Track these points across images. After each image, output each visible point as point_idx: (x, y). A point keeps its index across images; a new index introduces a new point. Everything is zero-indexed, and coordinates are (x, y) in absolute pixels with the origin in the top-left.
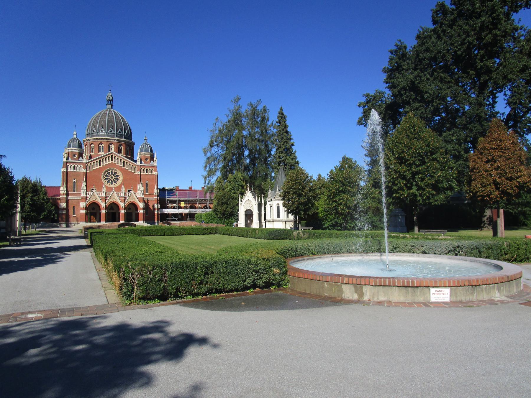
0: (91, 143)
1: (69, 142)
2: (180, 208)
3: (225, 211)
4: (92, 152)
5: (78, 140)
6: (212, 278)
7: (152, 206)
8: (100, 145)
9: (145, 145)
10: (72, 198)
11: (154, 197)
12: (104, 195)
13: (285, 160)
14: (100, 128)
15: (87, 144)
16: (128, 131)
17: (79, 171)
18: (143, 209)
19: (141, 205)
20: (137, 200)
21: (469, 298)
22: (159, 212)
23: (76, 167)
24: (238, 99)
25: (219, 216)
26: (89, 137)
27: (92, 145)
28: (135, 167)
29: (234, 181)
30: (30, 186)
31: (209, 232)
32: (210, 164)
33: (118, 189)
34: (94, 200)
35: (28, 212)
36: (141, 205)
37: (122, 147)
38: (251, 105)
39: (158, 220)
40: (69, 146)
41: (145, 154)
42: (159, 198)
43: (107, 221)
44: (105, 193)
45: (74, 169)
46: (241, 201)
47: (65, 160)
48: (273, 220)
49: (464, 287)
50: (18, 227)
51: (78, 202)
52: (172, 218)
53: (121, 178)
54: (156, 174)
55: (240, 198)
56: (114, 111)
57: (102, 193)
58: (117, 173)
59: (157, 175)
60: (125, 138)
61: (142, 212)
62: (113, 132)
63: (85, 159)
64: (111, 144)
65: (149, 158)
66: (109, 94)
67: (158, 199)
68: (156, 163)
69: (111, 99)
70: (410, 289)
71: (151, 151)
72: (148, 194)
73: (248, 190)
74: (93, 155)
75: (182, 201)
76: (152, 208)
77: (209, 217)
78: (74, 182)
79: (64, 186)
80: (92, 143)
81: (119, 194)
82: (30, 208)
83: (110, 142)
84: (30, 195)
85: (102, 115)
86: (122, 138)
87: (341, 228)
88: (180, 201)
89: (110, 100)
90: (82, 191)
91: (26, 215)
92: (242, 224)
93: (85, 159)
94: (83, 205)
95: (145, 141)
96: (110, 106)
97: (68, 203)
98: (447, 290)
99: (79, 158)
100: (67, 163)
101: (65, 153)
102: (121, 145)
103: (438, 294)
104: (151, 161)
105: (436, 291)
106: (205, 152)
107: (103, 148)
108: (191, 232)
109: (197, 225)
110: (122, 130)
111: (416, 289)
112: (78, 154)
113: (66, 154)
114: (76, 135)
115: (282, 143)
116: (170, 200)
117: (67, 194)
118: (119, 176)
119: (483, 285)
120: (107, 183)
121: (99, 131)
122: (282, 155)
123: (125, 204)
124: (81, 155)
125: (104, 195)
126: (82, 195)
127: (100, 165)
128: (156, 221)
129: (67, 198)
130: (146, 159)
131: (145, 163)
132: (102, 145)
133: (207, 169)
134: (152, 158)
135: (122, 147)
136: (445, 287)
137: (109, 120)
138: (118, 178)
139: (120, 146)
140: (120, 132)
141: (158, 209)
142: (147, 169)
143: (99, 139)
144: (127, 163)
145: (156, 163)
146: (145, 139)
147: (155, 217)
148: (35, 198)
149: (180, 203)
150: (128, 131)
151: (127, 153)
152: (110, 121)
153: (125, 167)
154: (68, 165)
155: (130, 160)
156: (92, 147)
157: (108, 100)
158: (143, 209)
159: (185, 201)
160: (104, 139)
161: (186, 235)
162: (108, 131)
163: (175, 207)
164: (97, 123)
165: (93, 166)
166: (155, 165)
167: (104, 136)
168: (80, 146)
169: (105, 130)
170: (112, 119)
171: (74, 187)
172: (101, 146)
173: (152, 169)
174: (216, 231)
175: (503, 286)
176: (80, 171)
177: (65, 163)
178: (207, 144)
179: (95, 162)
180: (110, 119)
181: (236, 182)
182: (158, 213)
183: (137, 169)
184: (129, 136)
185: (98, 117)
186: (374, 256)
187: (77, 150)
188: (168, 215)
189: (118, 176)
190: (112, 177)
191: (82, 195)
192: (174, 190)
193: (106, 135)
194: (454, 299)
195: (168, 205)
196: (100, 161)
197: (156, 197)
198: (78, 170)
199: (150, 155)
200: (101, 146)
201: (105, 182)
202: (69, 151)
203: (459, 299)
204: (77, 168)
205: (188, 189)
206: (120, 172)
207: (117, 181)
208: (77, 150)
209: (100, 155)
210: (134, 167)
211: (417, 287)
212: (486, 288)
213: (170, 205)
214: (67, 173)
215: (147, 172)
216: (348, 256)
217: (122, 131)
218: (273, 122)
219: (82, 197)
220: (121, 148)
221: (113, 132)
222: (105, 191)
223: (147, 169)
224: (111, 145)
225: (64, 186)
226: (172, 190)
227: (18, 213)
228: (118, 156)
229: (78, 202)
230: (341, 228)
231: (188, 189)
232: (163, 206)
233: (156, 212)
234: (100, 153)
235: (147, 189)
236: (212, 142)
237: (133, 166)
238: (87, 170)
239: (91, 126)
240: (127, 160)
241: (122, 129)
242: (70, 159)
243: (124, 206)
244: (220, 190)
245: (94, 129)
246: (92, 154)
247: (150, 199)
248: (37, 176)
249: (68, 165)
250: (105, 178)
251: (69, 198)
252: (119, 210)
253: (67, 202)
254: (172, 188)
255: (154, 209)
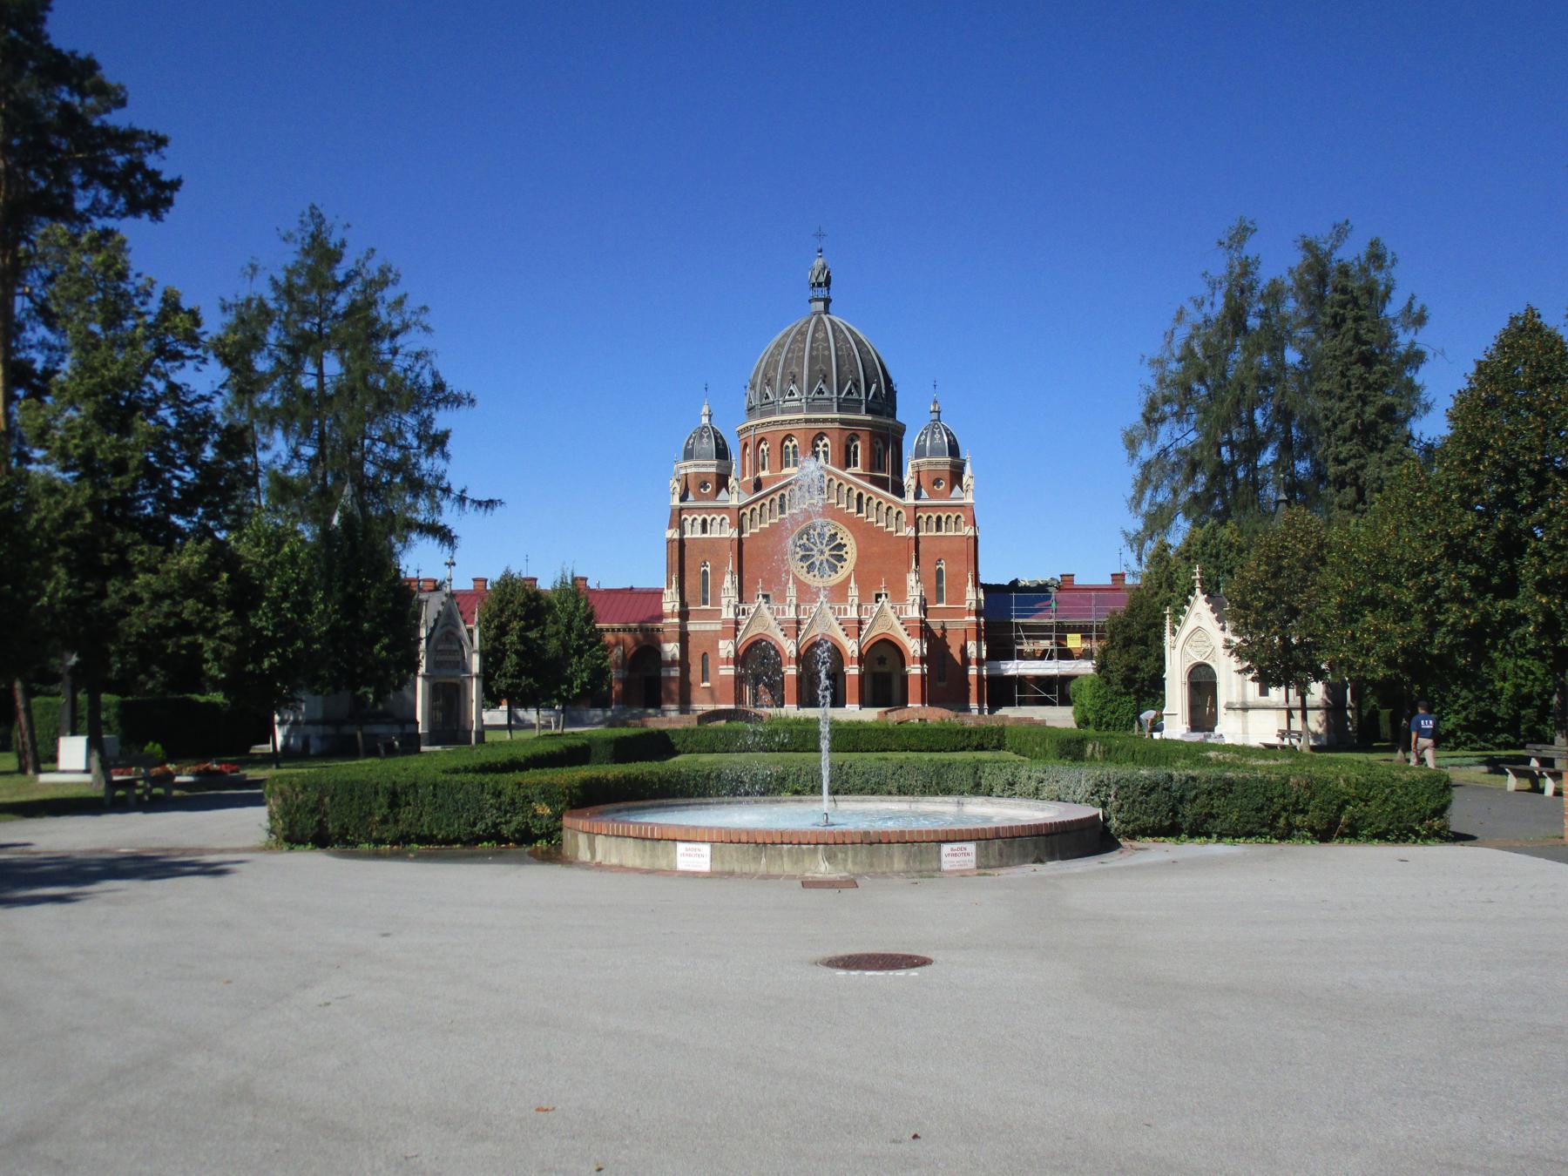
0: (758, 439)
1: (688, 443)
2: (1066, 654)
3: (1136, 669)
4: (764, 469)
5: (716, 433)
6: (406, 814)
7: (958, 648)
8: (787, 443)
9: (934, 433)
10: (697, 628)
11: (967, 618)
12: (852, 614)
13: (1363, 467)
14: (785, 386)
15: (747, 440)
16: (879, 387)
17: (717, 536)
18: (922, 660)
19: (914, 647)
20: (901, 628)
21: (749, 867)
22: (985, 673)
23: (709, 521)
24: (1242, 233)
25: (1115, 688)
26: (755, 418)
27: (762, 446)
28: (899, 513)
29: (1203, 554)
30: (520, 598)
31: (975, 740)
32: (1156, 489)
33: (839, 592)
34: (761, 631)
35: (512, 676)
36: (914, 647)
37: (858, 443)
38: (1308, 246)
39: (980, 702)
40: (688, 455)
41: (930, 463)
42: (982, 619)
43: (863, 703)
44: (855, 608)
45: (704, 530)
46: (1174, 632)
47: (676, 501)
48: (1244, 703)
49: (739, 845)
50: (474, 718)
51: (716, 637)
52: (1037, 692)
53: (851, 553)
54: (972, 533)
55: (1168, 622)
56: (831, 322)
57: (787, 608)
58: (839, 536)
59: (976, 538)
60: (868, 411)
61: (918, 672)
62: (826, 395)
63: (735, 496)
64: (820, 436)
65: (947, 476)
66: (818, 263)
67: (978, 624)
68: (970, 494)
69: (822, 279)
70: (648, 842)
71: (954, 450)
72: (944, 605)
73: (1198, 592)
74: (769, 477)
75: (1073, 630)
76: (958, 657)
77: (1102, 692)
78: (705, 572)
79: (674, 586)
80: (762, 439)
81: (840, 609)
82: (517, 664)
83: (818, 431)
84: (516, 625)
85: (794, 337)
86: (858, 411)
87: (1512, 739)
88: (1063, 630)
89: (820, 285)
90: (724, 601)
91: (509, 686)
92: (1178, 718)
93: (735, 496)
94: (726, 648)
95: (935, 416)
96: (821, 305)
97: (688, 641)
98: (706, 849)
99: (718, 491)
100: (681, 509)
101: (674, 479)
102: (853, 438)
103: (690, 855)
104: (952, 489)
105: (687, 849)
106: (1132, 443)
107: (795, 454)
108: (913, 741)
109: (947, 720)
110: (856, 384)
111: (655, 842)
112: (714, 479)
113: (678, 480)
114: (710, 416)
115: (1345, 404)
116: (1026, 627)
117: (684, 615)
118: (845, 545)
119: (782, 843)
120: (808, 572)
121: (782, 393)
122: (1344, 451)
123: (859, 646)
124: (722, 481)
125: (855, 615)
126: (724, 616)
127: (782, 510)
128: (973, 705)
129: (683, 627)
130: (937, 482)
131: (932, 495)
132: (791, 441)
133: (1145, 506)
134: (956, 476)
135: (858, 443)
136: (703, 842)
137: (815, 353)
138: (843, 553)
139: (852, 440)
140: (849, 392)
141: (979, 662)
142: (939, 518)
143: (782, 423)
144: (869, 499)
145: (970, 494)
146: (932, 409)
147: (968, 691)
148: (533, 634)
149: (1065, 638)
150: (879, 387)
151: (875, 462)
152: (817, 356)
153: (863, 515)
154: (686, 519)
155: (887, 490)
156: (763, 450)
157: (814, 284)
158: (922, 660)
159: (1086, 632)
160: (798, 421)
161: (895, 750)
162: (810, 392)
163: (1045, 651)
164: (776, 369)
165: (761, 516)
166: (969, 499)
167: (799, 410)
168: (722, 453)
169: (801, 391)
170: (824, 349)
171: (705, 591)
172: (791, 446)
173: (958, 517)
174: (998, 740)
175: (846, 853)
176: (723, 536)
177: (677, 513)
178: (1133, 416)
179: (767, 503)
180: (818, 349)
181: (1211, 556)
182: (979, 676)
183: (905, 520)
184: (885, 402)
185: (779, 345)
186: (946, 802)
187: (711, 465)
188: (1021, 680)
189: (840, 546)
190: (822, 553)
191: (724, 616)
192: (1051, 589)
193: (805, 405)
194: (718, 868)
195: (1022, 644)
196: (783, 496)
197: (973, 618)
198: (714, 533)
199: (948, 468)
200: (791, 446)
201: (797, 568)
202: (689, 471)
203: (727, 868)
204: (711, 525)
205: (1108, 581)
206: (848, 532)
207: (839, 565)
208: (710, 467)
209: (786, 476)
210: (894, 511)
211: (659, 840)
212: (789, 851)
213: (1027, 647)
214: (682, 542)
215: (939, 528)
216: (882, 801)
217: (856, 386)
218: (1410, 304)
219: (723, 623)
220: (856, 447)
221: (826, 395)
222: (794, 601)
223: (939, 518)
224: (822, 439)
225: (674, 586)
226: (1042, 588)
227: (474, 680)
228: (838, 477)
229: (716, 637)
230: (1512, 739)
231: (1108, 581)
232: (1001, 643)
233: (973, 671)
234: (786, 471)
235: (939, 590)
236: (1152, 406)
237: (889, 508)
238: (741, 531)
239: (759, 382)
240: (868, 491)
241: (859, 380)
242: (691, 497)
243: (794, 653)
244: (1160, 586)
245: (768, 391)
246: (763, 474)
247: (954, 624)
248: (564, 563)
249: (686, 519)
250: (798, 557)
251: (691, 628)
252: (903, 665)
253: (684, 638)
254: (1047, 579)
255: (966, 660)
